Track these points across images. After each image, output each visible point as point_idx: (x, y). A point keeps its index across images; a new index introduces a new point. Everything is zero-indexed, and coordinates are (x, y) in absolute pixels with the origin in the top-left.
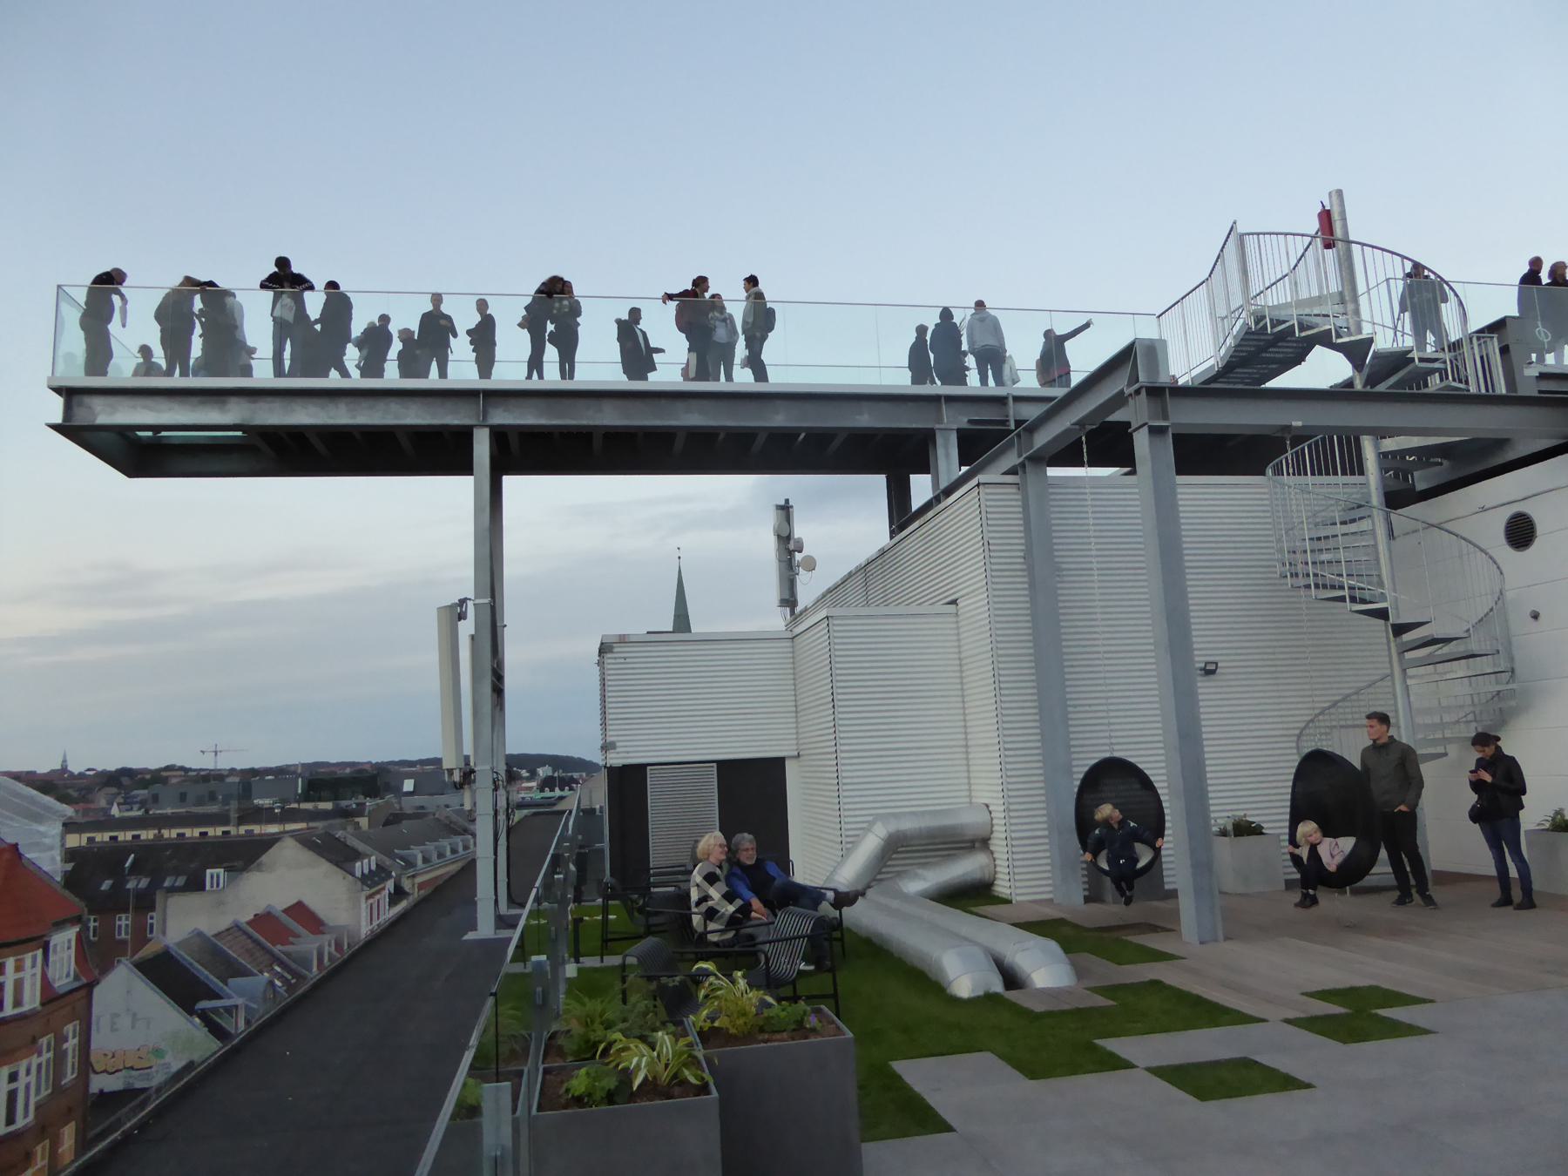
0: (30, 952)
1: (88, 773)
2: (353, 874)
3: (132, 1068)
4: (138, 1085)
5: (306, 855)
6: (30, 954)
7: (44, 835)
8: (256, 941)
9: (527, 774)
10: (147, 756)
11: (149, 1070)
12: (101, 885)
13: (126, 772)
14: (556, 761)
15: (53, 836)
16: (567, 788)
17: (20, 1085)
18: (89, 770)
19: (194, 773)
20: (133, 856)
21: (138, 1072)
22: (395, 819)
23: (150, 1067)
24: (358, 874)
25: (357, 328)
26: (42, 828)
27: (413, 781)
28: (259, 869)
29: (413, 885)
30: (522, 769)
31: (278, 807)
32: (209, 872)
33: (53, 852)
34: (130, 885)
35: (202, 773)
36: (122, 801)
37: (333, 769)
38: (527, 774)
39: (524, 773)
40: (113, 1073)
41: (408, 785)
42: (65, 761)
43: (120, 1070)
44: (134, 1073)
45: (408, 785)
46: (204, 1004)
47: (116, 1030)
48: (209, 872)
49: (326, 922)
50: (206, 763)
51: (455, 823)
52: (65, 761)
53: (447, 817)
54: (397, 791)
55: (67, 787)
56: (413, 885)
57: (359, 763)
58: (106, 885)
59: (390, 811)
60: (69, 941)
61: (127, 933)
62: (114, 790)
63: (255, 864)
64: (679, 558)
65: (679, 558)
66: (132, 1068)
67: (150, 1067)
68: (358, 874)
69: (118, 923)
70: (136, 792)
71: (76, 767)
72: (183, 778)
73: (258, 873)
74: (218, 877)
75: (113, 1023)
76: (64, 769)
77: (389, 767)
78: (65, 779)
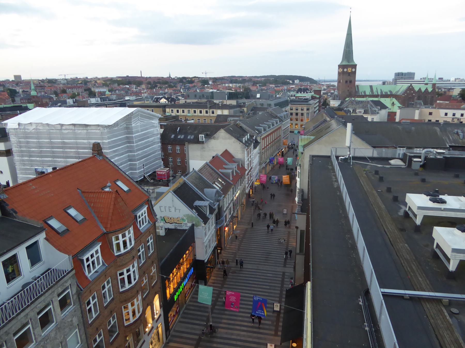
0: (95, 318)
1: (175, 78)
2: (242, 142)
3: (176, 223)
4: (178, 228)
5: (228, 135)
6: (127, 231)
7: (154, 123)
8: (213, 169)
9: (292, 82)
10: (189, 74)
11: (181, 225)
12: (171, 136)
13: (184, 78)
14: (302, 79)
15: (156, 124)
16: (305, 92)
17: (131, 272)
18: (176, 77)
19: (201, 79)
20: (179, 128)
21: (178, 225)
22: (255, 109)
23: (181, 224)
24: (244, 141)
25: (254, 206)
26: (153, 121)
27: (259, 94)
28: (214, 138)
29: (261, 139)
30: (290, 80)
31: (221, 104)
32: (200, 135)
33: (157, 128)
34: (179, 137)
35: (203, 79)
36: (184, 88)
37: (236, 78)
38: (292, 82)
39: (291, 82)
40: (171, 224)
41: (258, 96)
42: (170, 75)
43: (173, 223)
44: (176, 224)
45: (258, 96)
46: (197, 203)
47: (171, 211)
48: (200, 135)
49: (235, 157)
50: (203, 76)
51: (273, 114)
52: (170, 75)
53: (271, 112)
54: (255, 97)
55: (171, 82)
56: (261, 139)
57: (243, 77)
58: (173, 136)
59: (253, 106)
60: (145, 211)
61: (179, 151)
62: (181, 84)
63: (213, 137)
64: (351, 12)
65: (351, 12)
66: (176, 223)
67: (181, 224)
68: (244, 141)
69: (177, 148)
70: (187, 85)
71: (173, 76)
72: (198, 80)
73: (214, 140)
74: (203, 137)
75: (169, 210)
76: (170, 77)
77: (252, 78)
78: (170, 80)
